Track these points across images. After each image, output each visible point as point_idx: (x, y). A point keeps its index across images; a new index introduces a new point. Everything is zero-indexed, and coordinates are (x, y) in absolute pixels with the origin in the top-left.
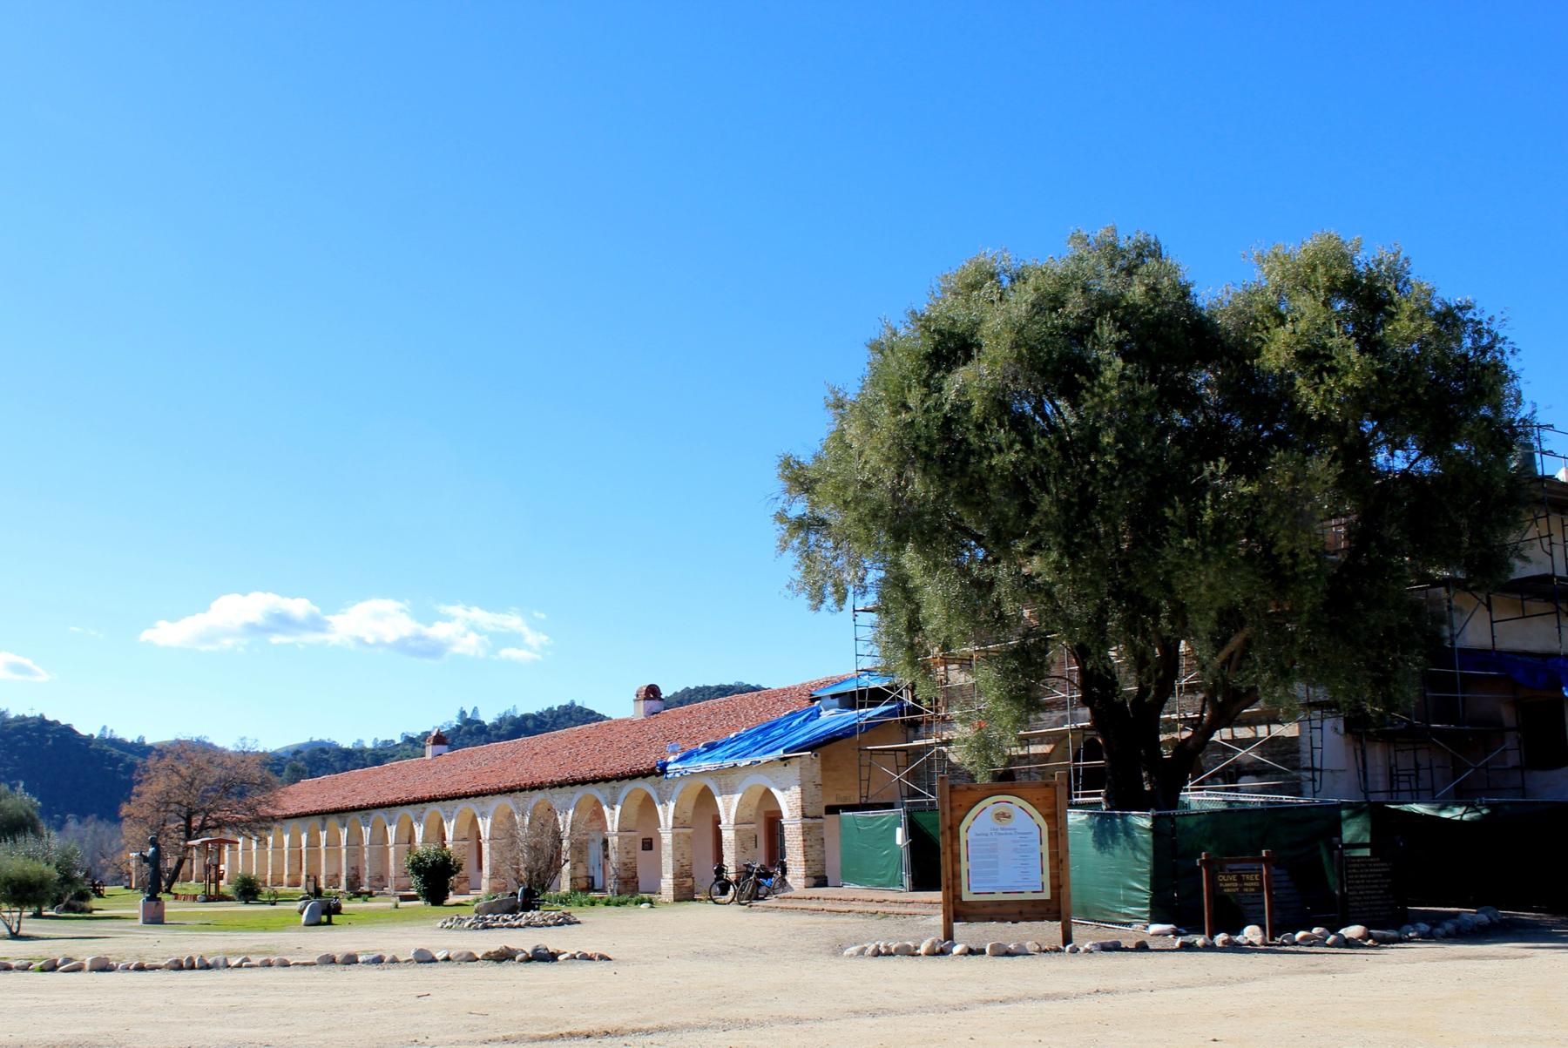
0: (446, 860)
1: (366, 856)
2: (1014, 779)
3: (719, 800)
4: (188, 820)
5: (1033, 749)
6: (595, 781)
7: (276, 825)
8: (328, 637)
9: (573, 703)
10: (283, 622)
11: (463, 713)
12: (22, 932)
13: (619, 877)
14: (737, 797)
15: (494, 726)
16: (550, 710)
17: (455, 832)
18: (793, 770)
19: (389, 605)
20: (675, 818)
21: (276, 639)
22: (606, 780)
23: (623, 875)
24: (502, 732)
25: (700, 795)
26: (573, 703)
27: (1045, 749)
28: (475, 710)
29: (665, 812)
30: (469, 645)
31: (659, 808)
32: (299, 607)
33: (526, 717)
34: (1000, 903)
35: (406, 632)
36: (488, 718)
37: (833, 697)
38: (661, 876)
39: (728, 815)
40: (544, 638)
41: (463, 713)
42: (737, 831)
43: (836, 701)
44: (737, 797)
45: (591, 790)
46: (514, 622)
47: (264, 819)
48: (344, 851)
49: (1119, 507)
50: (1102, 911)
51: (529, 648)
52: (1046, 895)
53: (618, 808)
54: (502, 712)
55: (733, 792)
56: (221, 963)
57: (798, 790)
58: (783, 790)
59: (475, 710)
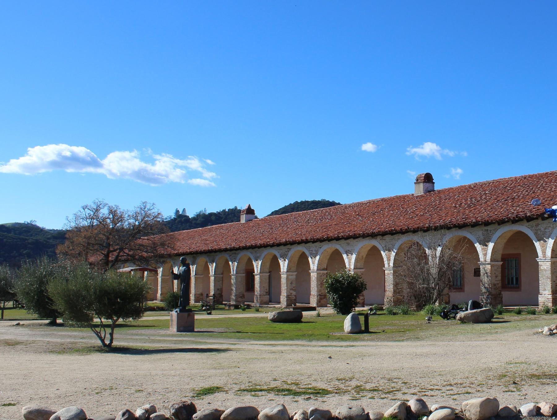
0: (141, 290)
1: (233, 281)
4: (107, 256)
6: (272, 246)
7: (168, 260)
8: (100, 171)
9: (236, 208)
10: (75, 159)
11: (177, 211)
12: (115, 343)
13: (490, 293)
15: (194, 219)
16: (224, 211)
17: (319, 264)
19: (127, 154)
20: (553, 251)
21: (70, 170)
22: (279, 245)
23: (494, 292)
24: (198, 222)
25: (301, 255)
26: (236, 208)
28: (184, 210)
29: (212, 267)
30: (176, 175)
31: (537, 245)
32: (81, 151)
33: (211, 214)
35: (136, 168)
36: (191, 214)
38: (537, 292)
39: (257, 268)
40: (214, 174)
41: (177, 211)
44: (318, 258)
45: (416, 238)
46: (194, 164)
47: (162, 256)
48: (212, 279)
51: (205, 179)
53: (491, 245)
54: (198, 211)
59: (184, 210)
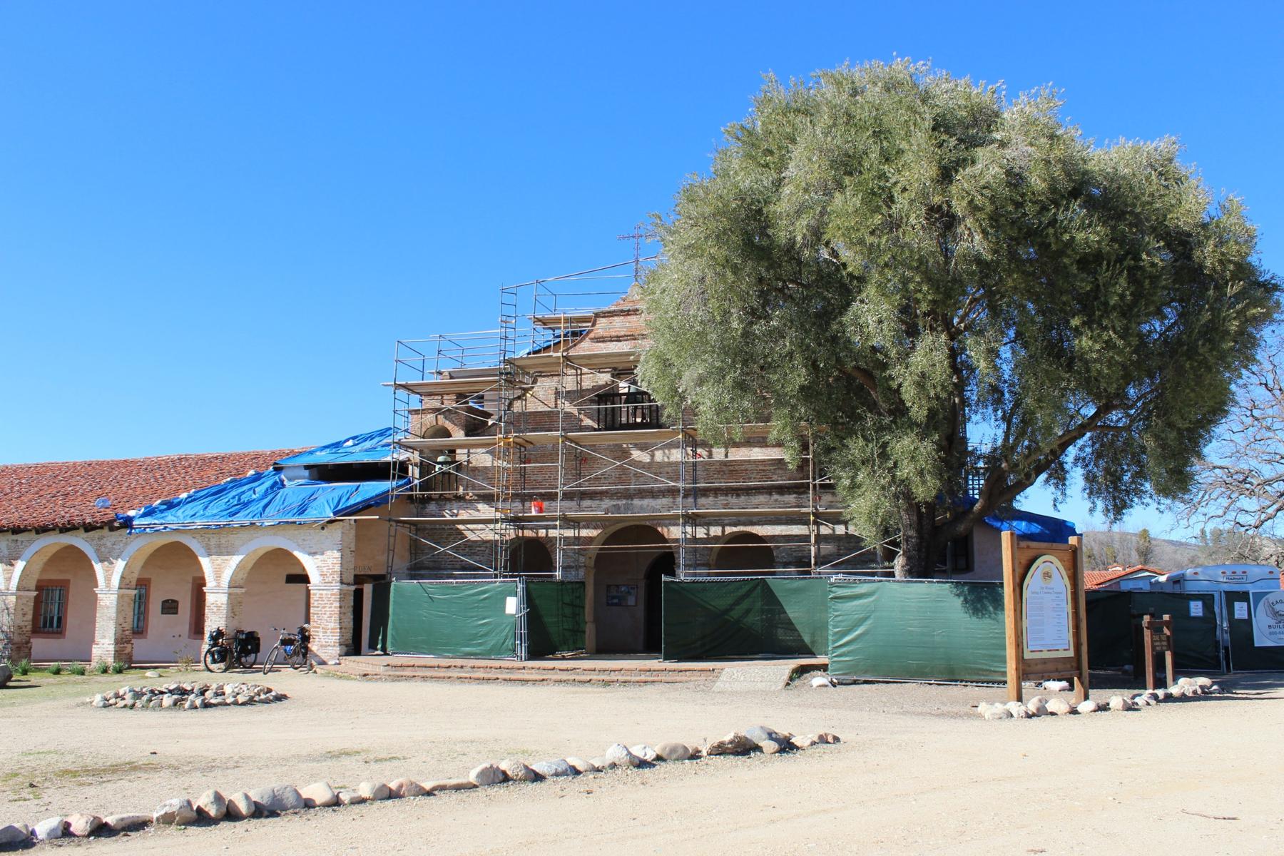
2: (356, 576)
3: (205, 562)
5: (585, 533)
14: (235, 560)
18: (336, 533)
20: (122, 577)
23: (17, 638)
27: (593, 533)
31: (99, 568)
34: (1045, 661)
37: (307, 467)
38: (91, 641)
42: (230, 594)
43: (306, 473)
49: (875, 276)
50: (978, 671)
52: (1071, 654)
55: (230, 553)
56: (290, 799)
57: (338, 555)
58: (313, 554)
